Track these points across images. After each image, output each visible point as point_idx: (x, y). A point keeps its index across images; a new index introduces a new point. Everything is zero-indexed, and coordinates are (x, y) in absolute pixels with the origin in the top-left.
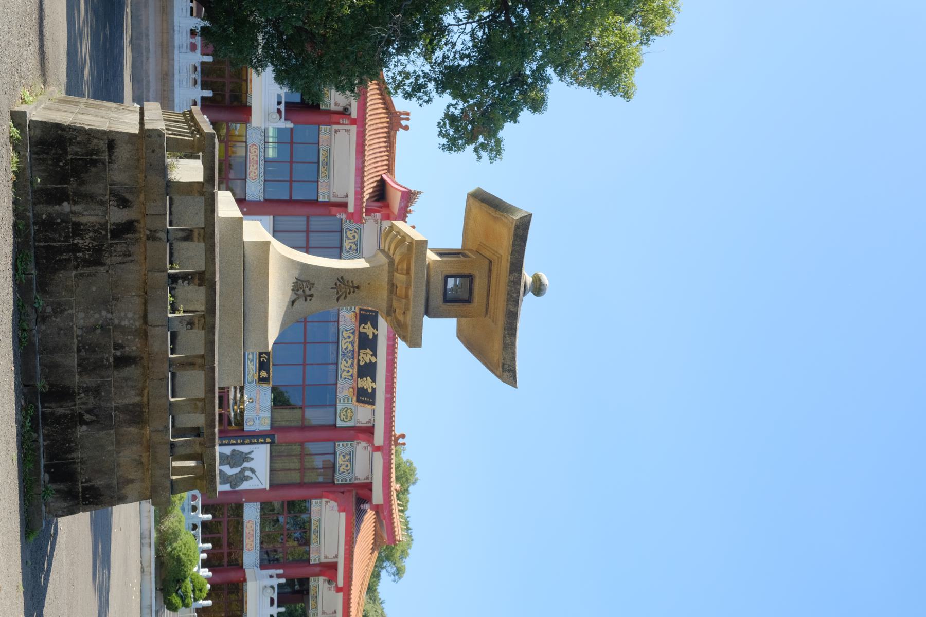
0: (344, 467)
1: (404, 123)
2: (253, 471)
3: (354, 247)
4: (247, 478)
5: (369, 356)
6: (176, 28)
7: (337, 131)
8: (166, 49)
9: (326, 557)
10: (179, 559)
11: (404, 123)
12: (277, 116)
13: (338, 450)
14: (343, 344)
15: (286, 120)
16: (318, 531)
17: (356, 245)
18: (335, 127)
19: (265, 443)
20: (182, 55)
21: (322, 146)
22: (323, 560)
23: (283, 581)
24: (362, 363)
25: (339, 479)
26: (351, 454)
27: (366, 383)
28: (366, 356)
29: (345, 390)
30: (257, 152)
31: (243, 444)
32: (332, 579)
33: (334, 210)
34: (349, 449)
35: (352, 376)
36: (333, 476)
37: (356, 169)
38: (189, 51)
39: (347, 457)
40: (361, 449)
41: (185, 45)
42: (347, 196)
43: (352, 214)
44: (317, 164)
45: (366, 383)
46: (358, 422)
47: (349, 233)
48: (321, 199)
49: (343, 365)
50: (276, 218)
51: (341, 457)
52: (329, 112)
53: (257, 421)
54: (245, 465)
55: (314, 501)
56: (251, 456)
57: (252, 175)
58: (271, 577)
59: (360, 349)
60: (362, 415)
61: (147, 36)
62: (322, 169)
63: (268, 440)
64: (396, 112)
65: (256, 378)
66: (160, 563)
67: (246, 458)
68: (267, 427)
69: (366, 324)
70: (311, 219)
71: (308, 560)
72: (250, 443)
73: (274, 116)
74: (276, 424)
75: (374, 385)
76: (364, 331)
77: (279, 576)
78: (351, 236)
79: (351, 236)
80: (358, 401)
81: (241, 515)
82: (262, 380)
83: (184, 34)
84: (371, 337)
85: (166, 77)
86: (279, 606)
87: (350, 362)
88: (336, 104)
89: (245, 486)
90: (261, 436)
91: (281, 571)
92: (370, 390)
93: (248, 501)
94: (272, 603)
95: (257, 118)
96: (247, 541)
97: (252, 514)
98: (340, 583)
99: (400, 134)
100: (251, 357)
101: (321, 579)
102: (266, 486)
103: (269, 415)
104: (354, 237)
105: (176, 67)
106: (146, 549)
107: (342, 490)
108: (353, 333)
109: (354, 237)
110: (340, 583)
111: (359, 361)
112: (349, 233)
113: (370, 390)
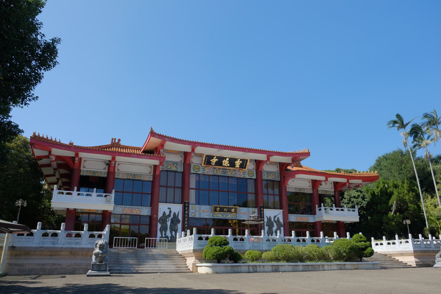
1: (117, 141)
2: (275, 217)
3: (175, 165)
4: (278, 219)
5: (226, 161)
6: (40, 245)
7: (118, 170)
8: (53, 252)
9: (310, 186)
10: (350, 249)
11: (117, 141)
12: (108, 198)
13: (266, 178)
14: (220, 173)
15: (111, 193)
16: (300, 189)
17: (174, 164)
18: (116, 170)
19: (263, 211)
20: (59, 242)
21: (125, 177)
22: (311, 187)
24: (229, 165)
25: (278, 179)
26: (268, 172)
27: (238, 163)
29: (240, 174)
30: (126, 209)
33: (157, 173)
34: (265, 174)
36: (277, 181)
38: (56, 238)
39: (269, 174)
40: (266, 168)
41: (52, 240)
43: (160, 163)
44: (134, 181)
45: (238, 163)
46: (254, 169)
47: (168, 167)
48: (151, 179)
49: (229, 174)
50: (160, 201)
52: (108, 173)
54: (272, 220)
55: (287, 190)
56: (269, 217)
57: (138, 212)
58: (320, 210)
60: (250, 166)
61: (43, 265)
62: (137, 178)
63: (262, 209)
64: (111, 144)
66: (349, 259)
67: (269, 219)
68: (256, 210)
69: (211, 162)
70: (161, 185)
72: (264, 217)
73: (108, 198)
74: (254, 205)
76: (214, 163)
78: (170, 166)
79: (170, 166)
80: (245, 168)
81: (293, 223)
82: (236, 212)
83: (45, 240)
84: (217, 160)
85: (73, 252)
87: (228, 171)
88: (105, 169)
89: (281, 220)
91: (317, 206)
92: (241, 162)
93: (288, 219)
95: (110, 207)
96: (304, 220)
97: (293, 218)
99: (122, 143)
100: (225, 216)
102: (281, 211)
103: (251, 208)
104: (170, 165)
105: (67, 246)
106: (347, 267)
107: (283, 177)
108: (215, 168)
109: (170, 165)
110: (322, 178)
111: (227, 166)
112: (168, 167)
113: (241, 162)
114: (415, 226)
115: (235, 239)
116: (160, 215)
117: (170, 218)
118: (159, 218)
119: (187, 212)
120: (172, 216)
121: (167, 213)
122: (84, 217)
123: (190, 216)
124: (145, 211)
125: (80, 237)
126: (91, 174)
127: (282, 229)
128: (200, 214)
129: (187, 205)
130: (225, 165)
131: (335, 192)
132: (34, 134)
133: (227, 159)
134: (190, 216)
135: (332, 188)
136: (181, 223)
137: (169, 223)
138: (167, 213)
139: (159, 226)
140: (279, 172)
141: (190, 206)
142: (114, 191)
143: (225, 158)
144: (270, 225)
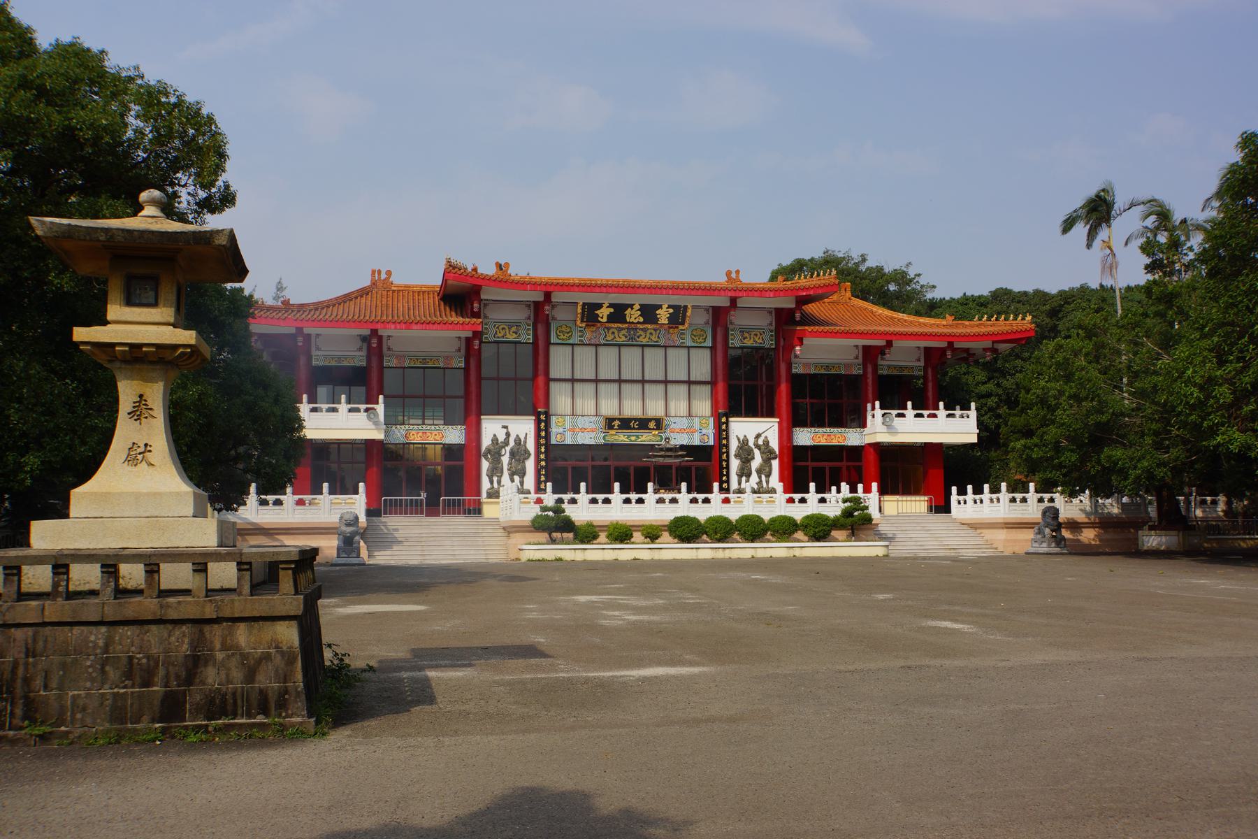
1: (383, 276)
2: (758, 436)
3: (514, 329)
4: (767, 443)
7: (389, 349)
9: (857, 358)
11: (383, 276)
16: (827, 367)
18: (385, 348)
19: (727, 423)
22: (860, 360)
23: (877, 404)
24: (641, 320)
28: (633, 315)
31: (727, 446)
32: (881, 351)
37: (408, 328)
42: (460, 338)
44: (425, 367)
45: (663, 315)
46: (707, 323)
48: (463, 365)
53: (704, 431)
54: (751, 444)
57: (438, 437)
59: (625, 322)
63: (724, 420)
67: (744, 444)
71: (361, 368)
72: (727, 438)
77: (873, 409)
87: (641, 332)
89: (774, 444)
90: (720, 427)
91: (869, 406)
92: (671, 311)
94: (903, 416)
96: (835, 442)
97: (804, 437)
98: (881, 343)
101: (880, 362)
108: (608, 329)
113: (671, 311)
115: (1013, 500)
116: (486, 442)
117: (508, 449)
118: (483, 449)
119: (543, 434)
120: (512, 443)
121: (501, 438)
122: (297, 717)
123: (553, 441)
124: (455, 435)
126: (333, 363)
127: (775, 464)
128: (575, 438)
129: (543, 417)
131: (925, 368)
132: (57, 40)
134: (553, 441)
135: (918, 360)
136: (532, 458)
137: (505, 459)
138: (501, 438)
139: (485, 465)
140: (773, 328)
141: (553, 419)
142: (381, 397)
143: (631, 306)
144: (745, 454)
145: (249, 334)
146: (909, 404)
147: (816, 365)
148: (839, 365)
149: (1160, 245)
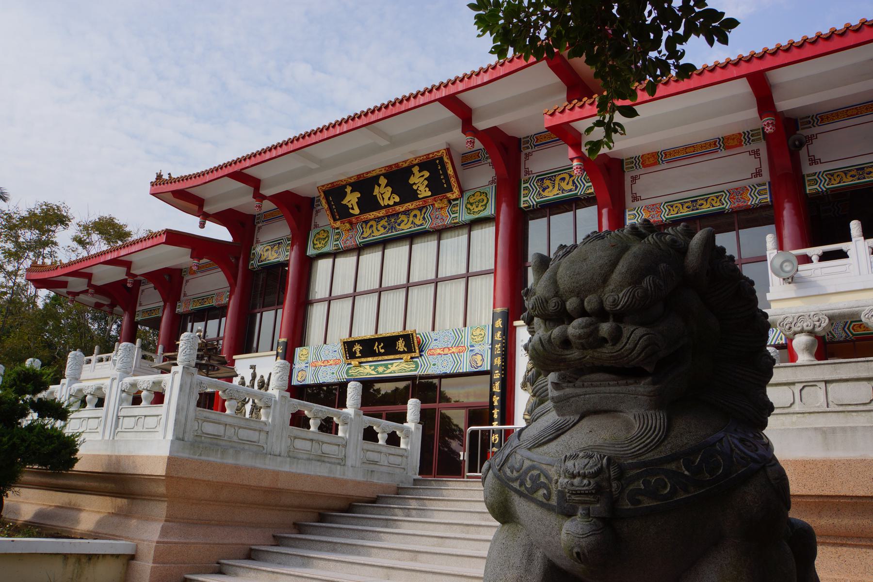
0: (564, 185)
5: (382, 190)
35: (420, 209)
39: (547, 183)
51: (546, 193)
53: (477, 349)
65: (407, 357)
75: (815, 258)
86: (848, 239)
92: (427, 174)
100: (381, 369)
111: (396, 204)
114: (13, 226)
125: (847, 257)
128: (316, 374)
130: (386, 202)
133: (383, 181)
145: (494, 165)
146: (855, 227)
147: (670, 204)
148: (718, 195)
149: (99, 326)
